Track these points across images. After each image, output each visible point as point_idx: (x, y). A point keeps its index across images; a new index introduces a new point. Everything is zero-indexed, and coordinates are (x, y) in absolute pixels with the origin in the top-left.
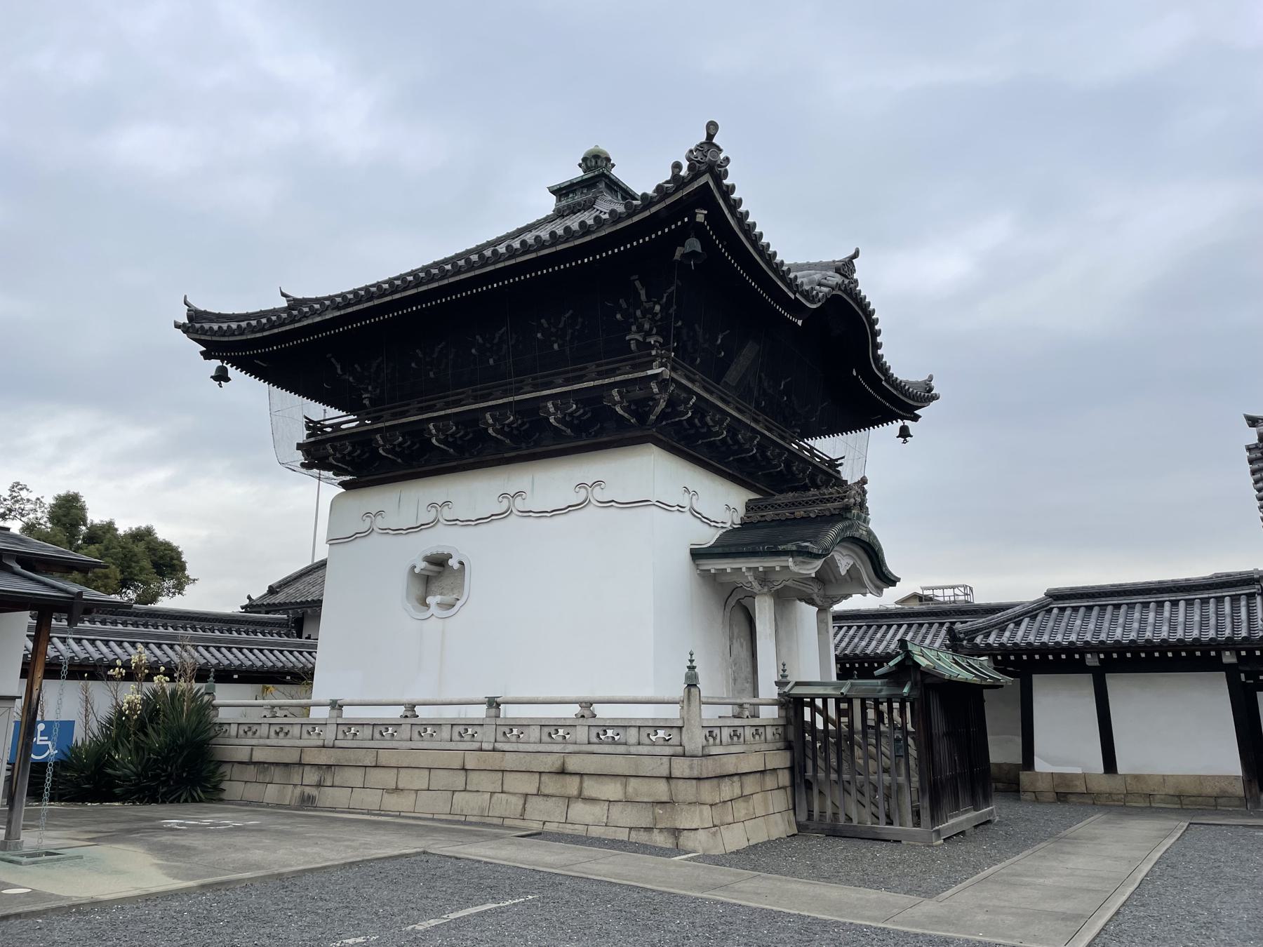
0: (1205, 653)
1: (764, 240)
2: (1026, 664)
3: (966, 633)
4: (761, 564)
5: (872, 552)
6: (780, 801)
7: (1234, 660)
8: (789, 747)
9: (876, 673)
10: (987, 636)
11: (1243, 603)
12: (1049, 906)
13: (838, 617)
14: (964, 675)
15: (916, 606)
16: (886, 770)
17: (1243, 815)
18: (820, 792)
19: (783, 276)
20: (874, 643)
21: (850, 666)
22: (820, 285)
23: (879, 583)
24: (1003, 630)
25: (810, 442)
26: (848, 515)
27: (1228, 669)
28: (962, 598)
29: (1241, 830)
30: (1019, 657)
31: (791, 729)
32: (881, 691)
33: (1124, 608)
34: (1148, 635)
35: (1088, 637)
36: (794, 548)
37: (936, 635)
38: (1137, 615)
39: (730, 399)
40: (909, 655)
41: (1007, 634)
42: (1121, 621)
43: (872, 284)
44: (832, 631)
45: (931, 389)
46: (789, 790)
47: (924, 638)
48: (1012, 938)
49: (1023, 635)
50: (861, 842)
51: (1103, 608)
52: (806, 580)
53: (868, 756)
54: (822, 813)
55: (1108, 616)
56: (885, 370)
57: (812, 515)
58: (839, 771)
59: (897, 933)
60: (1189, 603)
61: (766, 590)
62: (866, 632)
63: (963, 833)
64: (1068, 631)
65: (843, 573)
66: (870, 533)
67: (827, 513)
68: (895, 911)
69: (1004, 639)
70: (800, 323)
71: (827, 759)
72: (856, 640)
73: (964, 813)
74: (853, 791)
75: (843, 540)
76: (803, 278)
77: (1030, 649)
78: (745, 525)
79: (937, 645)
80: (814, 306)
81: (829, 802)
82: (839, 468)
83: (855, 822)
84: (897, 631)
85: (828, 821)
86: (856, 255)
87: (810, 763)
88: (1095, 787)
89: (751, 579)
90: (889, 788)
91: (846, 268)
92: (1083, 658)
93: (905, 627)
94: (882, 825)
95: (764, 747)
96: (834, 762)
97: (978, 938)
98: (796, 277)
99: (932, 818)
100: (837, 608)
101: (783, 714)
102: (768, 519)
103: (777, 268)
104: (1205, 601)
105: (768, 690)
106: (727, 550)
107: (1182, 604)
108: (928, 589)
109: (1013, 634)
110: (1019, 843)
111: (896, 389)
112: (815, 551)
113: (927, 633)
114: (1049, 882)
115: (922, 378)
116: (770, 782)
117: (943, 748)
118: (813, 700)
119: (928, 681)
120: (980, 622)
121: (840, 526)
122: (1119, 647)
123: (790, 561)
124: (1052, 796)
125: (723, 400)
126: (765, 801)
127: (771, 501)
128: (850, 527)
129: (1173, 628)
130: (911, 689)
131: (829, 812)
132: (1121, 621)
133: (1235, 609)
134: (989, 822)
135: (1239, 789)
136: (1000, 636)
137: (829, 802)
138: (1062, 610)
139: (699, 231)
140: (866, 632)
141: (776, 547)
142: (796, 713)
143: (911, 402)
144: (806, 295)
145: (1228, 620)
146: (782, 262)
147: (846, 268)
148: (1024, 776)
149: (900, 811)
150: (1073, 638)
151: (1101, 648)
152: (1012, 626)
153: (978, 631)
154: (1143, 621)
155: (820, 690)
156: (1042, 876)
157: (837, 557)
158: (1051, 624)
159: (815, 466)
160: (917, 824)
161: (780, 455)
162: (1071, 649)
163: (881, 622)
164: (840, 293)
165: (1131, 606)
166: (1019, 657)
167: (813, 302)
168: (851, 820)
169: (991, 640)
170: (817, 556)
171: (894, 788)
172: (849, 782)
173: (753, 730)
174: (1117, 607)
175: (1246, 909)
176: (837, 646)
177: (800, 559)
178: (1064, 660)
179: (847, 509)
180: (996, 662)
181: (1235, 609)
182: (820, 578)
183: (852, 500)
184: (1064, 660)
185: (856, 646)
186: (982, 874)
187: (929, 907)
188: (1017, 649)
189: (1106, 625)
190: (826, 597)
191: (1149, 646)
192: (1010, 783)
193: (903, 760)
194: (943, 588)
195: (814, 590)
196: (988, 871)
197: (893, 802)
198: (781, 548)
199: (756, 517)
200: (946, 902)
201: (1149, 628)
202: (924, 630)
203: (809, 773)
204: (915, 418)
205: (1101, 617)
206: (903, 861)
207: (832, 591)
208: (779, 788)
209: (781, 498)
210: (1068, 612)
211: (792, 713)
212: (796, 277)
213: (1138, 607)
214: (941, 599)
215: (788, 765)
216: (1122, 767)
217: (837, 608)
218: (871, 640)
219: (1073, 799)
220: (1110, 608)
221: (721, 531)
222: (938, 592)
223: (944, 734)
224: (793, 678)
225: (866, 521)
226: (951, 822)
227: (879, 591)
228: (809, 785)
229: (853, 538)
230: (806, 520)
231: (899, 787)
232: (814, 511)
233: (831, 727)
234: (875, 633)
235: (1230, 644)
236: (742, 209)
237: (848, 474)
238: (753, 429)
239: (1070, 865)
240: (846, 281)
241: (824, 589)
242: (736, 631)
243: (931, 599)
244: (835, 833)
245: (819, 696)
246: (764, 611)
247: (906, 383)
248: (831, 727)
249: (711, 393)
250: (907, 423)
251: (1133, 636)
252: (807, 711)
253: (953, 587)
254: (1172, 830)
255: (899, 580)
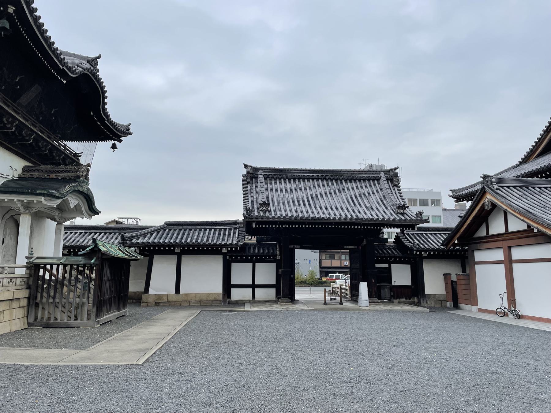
0: (217, 248)
1: (48, 34)
2: (151, 252)
3: (129, 238)
4: (26, 199)
5: (89, 199)
6: (20, 313)
7: (226, 251)
8: (29, 287)
9: (79, 253)
10: (138, 239)
11: (232, 231)
12: (135, 347)
13: (66, 228)
14: (121, 255)
15: (113, 225)
16: (79, 297)
17: (220, 307)
18: (43, 308)
19: (58, 56)
20: (87, 240)
21: (70, 250)
22: (78, 66)
23: (90, 213)
24: (145, 237)
25: (65, 143)
26: (78, 180)
27: (225, 255)
28: (135, 223)
29: (218, 312)
30: (149, 248)
31: (31, 279)
32: (81, 261)
33: (193, 230)
34: (199, 241)
35: (177, 241)
36: (46, 192)
37: (116, 238)
38: (197, 233)
39: (20, 112)
40: (96, 245)
41: (146, 238)
42: (191, 235)
43: (104, 72)
44: (63, 233)
45: (129, 130)
46: (26, 308)
47: (111, 239)
48: (115, 361)
49: (153, 239)
50: (61, 329)
51: (185, 230)
52: (52, 208)
53: (70, 291)
54: (42, 318)
55: (186, 233)
56: (107, 116)
57: (59, 178)
58: (54, 298)
59: (62, 366)
60: (215, 230)
61: (27, 211)
62: (84, 235)
63: (110, 321)
64: (170, 238)
65: (72, 206)
66: (88, 190)
67: (68, 178)
68: (65, 357)
69: (145, 241)
70: (65, 82)
71: (48, 293)
72: (78, 239)
73: (112, 313)
74: (60, 306)
75: (74, 191)
76: (68, 59)
77: (154, 245)
78: (21, 178)
79: (116, 242)
80: (73, 76)
81: (46, 312)
82: (79, 158)
83: (59, 321)
84: (99, 235)
85: (45, 321)
86: (99, 57)
87: (39, 295)
88: (170, 299)
89: (19, 205)
90: (78, 304)
91: (93, 62)
92: (174, 249)
93: (103, 234)
94: (72, 321)
95: (14, 288)
96: (52, 293)
97: (100, 363)
98: (64, 58)
99: (97, 316)
100: (67, 223)
101: (28, 272)
102: (35, 177)
103: (55, 51)
104: (220, 230)
105: (21, 260)
106: (7, 190)
107: (213, 230)
108: (121, 218)
109: (149, 239)
110: (133, 323)
111: (112, 126)
112: (57, 195)
113: (113, 237)
114: (139, 337)
115: (126, 123)
116: (15, 304)
117: (107, 286)
118: (45, 265)
119: (104, 257)
120: (135, 233)
121: (73, 184)
122: (188, 245)
123: (42, 199)
124: (154, 303)
125: (15, 112)
126: (11, 314)
127: (38, 168)
128: (78, 186)
129: (208, 239)
130: (95, 261)
131: (46, 317)
132: (191, 235)
133: (229, 233)
134: (124, 316)
135: (220, 298)
136: (143, 239)
137: (46, 312)
138: (170, 230)
139: (9, 17)
140: (84, 235)
141: (35, 191)
142: (35, 272)
143: (119, 133)
144: (70, 69)
145: (227, 237)
146: (57, 48)
147: (93, 62)
148: (144, 297)
149: (81, 316)
150: (172, 241)
151: (182, 245)
152: (149, 235)
153: (134, 237)
154: (198, 236)
155: (54, 261)
156: (138, 335)
157: (69, 199)
158: (165, 235)
159: (65, 154)
160: (88, 319)
161: (46, 146)
162: (171, 245)
163: (92, 231)
164: (88, 73)
165: (195, 230)
166: (149, 248)
167: (72, 73)
168: (57, 319)
169: (139, 241)
170: (58, 198)
171: (81, 304)
172: (58, 303)
173: (9, 280)
174: (190, 230)
175: (208, 341)
176: (64, 240)
177: (48, 198)
178: (166, 250)
179: (78, 177)
180: (140, 250)
181: (229, 233)
182: (59, 208)
183: (81, 173)
184: (166, 250)
185: (78, 242)
186: (113, 337)
187: (83, 353)
188: (149, 245)
189: (185, 236)
190: (62, 218)
191: (199, 245)
192: (137, 300)
193: (87, 292)
194: (128, 218)
195: (56, 214)
196: (116, 335)
197: (79, 310)
198: (38, 192)
199: (28, 175)
200: (92, 351)
201: (200, 239)
202: (111, 236)
203: (38, 300)
204: (120, 141)
205: (184, 233)
206: (78, 335)
207: (65, 215)
208: (20, 307)
209: (43, 167)
210: (172, 231)
211: (33, 272)
212: (64, 58)
213: (198, 230)
214: (126, 223)
215: (27, 296)
216: (182, 291)
217: (67, 223)
218: (86, 239)
219: (161, 304)
220: (188, 230)
221: (5, 180)
222: (125, 220)
223: (109, 280)
224: (35, 255)
225: (87, 184)
226: (105, 317)
227: (90, 217)
228: (37, 305)
229: (79, 191)
230: (56, 180)
231: (83, 304)
232: (61, 176)
233: (53, 278)
234: (88, 236)
235: (226, 246)
236: (37, 14)
237: (83, 161)
238: (32, 130)
239: (150, 330)
240: (92, 68)
241: (62, 213)
242: (8, 231)
243: (121, 223)
244: (47, 326)
245: (48, 264)
246: (25, 222)
247: (118, 124)
248: (53, 278)
249: (8, 106)
250: (116, 142)
251: (194, 241)
252: (41, 271)
253: (132, 219)
254: (194, 314)
255: (100, 212)
